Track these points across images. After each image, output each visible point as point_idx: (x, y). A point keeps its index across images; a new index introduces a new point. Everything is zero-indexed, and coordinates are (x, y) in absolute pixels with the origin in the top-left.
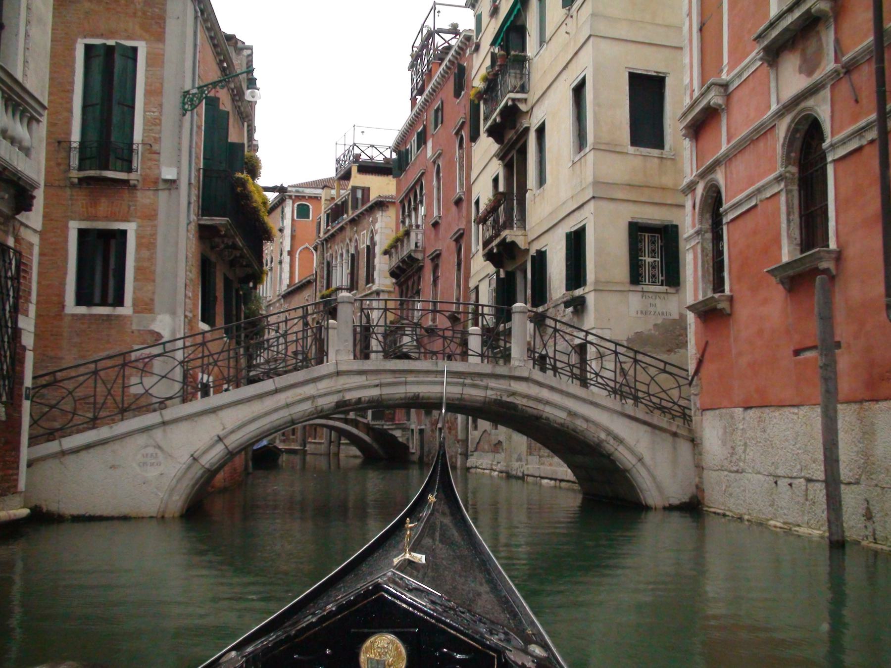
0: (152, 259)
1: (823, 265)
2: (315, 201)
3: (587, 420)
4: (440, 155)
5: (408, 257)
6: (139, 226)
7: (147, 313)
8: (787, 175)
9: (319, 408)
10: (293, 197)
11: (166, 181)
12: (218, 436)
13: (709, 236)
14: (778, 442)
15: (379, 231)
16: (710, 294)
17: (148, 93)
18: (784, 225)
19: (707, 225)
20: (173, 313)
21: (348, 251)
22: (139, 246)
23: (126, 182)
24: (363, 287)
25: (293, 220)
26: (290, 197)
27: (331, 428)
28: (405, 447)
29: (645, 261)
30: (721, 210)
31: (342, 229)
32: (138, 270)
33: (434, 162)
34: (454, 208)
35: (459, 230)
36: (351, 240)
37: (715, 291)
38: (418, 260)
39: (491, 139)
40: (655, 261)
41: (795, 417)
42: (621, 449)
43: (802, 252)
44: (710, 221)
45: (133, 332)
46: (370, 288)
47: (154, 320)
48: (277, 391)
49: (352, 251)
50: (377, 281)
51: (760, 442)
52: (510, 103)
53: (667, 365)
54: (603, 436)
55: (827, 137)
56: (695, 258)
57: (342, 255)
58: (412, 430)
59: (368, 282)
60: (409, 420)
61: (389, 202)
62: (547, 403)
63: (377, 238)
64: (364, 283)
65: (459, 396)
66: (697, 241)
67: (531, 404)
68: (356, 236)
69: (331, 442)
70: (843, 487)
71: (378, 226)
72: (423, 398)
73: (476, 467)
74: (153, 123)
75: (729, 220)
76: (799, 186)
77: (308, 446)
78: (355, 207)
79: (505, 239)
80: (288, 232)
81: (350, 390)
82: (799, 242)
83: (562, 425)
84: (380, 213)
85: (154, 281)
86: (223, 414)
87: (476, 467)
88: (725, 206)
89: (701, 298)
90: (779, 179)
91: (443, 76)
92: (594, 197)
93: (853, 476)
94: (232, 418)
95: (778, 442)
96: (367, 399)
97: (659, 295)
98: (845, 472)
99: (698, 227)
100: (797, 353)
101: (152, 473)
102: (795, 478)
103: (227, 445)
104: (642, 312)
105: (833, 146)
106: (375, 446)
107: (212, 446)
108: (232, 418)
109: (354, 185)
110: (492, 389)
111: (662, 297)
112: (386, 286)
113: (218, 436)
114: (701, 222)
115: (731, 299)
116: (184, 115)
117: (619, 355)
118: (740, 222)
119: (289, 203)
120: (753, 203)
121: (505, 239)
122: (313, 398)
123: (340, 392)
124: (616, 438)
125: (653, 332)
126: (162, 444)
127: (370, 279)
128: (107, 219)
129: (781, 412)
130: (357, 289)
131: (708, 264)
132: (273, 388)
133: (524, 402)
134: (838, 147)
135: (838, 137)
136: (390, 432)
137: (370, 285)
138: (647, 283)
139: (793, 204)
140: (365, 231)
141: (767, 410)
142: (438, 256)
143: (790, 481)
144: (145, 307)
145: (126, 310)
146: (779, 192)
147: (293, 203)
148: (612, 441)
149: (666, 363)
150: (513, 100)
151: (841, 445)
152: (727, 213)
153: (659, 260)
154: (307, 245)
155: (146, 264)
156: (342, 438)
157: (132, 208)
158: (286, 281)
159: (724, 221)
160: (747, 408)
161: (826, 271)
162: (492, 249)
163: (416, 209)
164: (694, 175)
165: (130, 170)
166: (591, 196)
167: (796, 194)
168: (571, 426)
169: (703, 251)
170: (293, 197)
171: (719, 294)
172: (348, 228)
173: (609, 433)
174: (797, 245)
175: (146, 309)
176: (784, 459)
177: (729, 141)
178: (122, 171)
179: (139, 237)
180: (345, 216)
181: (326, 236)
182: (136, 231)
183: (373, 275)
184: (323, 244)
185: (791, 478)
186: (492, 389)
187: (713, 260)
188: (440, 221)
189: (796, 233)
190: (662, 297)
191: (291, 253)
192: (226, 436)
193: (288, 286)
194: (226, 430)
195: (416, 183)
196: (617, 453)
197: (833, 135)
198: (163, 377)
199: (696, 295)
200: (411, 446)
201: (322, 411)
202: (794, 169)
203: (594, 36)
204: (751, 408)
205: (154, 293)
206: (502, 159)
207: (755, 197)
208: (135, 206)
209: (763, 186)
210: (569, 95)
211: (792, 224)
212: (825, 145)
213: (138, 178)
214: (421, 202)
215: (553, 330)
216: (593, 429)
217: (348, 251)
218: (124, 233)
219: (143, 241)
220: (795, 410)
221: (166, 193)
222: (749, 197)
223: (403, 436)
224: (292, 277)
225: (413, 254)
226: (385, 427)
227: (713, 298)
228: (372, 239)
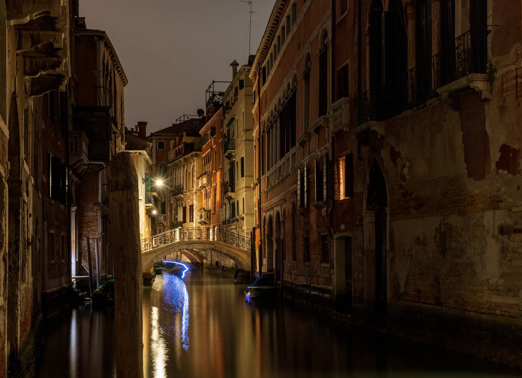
10: (156, 139)
25: (156, 149)
140: (190, 164)
150: (230, 152)
170: (156, 139)
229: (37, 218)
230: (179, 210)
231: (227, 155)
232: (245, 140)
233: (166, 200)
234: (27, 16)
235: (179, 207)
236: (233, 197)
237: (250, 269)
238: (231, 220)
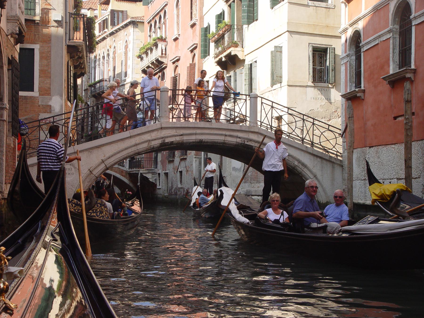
0: (49, 65)
1: (408, 75)
5: (156, 61)
6: (41, 47)
7: (47, 95)
8: (394, 29)
9: (152, 147)
12: (102, 160)
13: (354, 58)
14: (385, 163)
16: (353, 89)
18: (391, 55)
19: (353, 52)
22: (41, 58)
29: (316, 68)
30: (361, 45)
32: (41, 71)
34: (190, 30)
35: (194, 44)
37: (356, 87)
40: (321, 68)
41: (393, 149)
42: (305, 170)
43: (399, 69)
44: (354, 50)
45: (39, 106)
47: (51, 99)
48: (131, 137)
51: (377, 163)
53: (330, 127)
54: (296, 163)
55: (413, 13)
56: (346, 69)
58: (159, 174)
60: (156, 168)
61: (138, 22)
65: (223, 141)
66: (347, 60)
70: (413, 180)
72: (204, 142)
75: (364, 51)
76: (400, 35)
78: (113, 24)
82: (398, 64)
85: (50, 77)
86: (104, 148)
88: (363, 43)
89: (348, 91)
90: (390, 31)
93: (418, 174)
94: (109, 151)
95: (385, 163)
96: (176, 142)
97: (324, 88)
98: (414, 173)
99: (348, 52)
100: (395, 118)
102: (392, 179)
103: (106, 164)
104: (314, 98)
105: (415, 18)
107: (99, 165)
108: (109, 151)
110: (240, 138)
111: (325, 90)
113: (102, 160)
114: (350, 51)
115: (364, 91)
117: (305, 121)
118: (370, 51)
120: (377, 43)
121: (230, 53)
122: (149, 141)
123: (162, 138)
124: (303, 164)
125: (319, 109)
129: (386, 148)
131: (353, 73)
132: (129, 135)
134: (417, 18)
135: (417, 14)
138: (317, 81)
139: (396, 45)
140: (121, 41)
141: (380, 147)
142: (178, 60)
143: (390, 181)
145: (35, 93)
146: (389, 38)
148: (301, 166)
149: (329, 125)
151: (413, 160)
152: (363, 47)
153: (324, 68)
155: (46, 68)
157: (37, 36)
159: (362, 50)
160: (370, 147)
161: (409, 79)
162: (222, 58)
164: (346, 24)
166: (287, 30)
167: (398, 40)
169: (350, 66)
171: (359, 89)
173: (299, 161)
174: (397, 65)
175: (46, 93)
176: (387, 171)
177: (365, 10)
179: (41, 53)
182: (39, 49)
185: (391, 179)
186: (240, 138)
187: (356, 71)
188: (179, 37)
189: (397, 58)
190: (325, 90)
192: (106, 160)
194: (106, 157)
196: (303, 172)
197: (415, 13)
198: (240, 110)
199: (346, 90)
200: (158, 184)
201: (153, 148)
202: (397, 27)
204: (373, 147)
205: (50, 84)
207: (378, 39)
208: (38, 35)
209: (382, 34)
211: (395, 54)
212: (411, 17)
215: (271, 107)
218: (33, 49)
219: (44, 55)
220: (393, 146)
222: (375, 39)
225: (160, 59)
227: (355, 90)
236: (241, 57)
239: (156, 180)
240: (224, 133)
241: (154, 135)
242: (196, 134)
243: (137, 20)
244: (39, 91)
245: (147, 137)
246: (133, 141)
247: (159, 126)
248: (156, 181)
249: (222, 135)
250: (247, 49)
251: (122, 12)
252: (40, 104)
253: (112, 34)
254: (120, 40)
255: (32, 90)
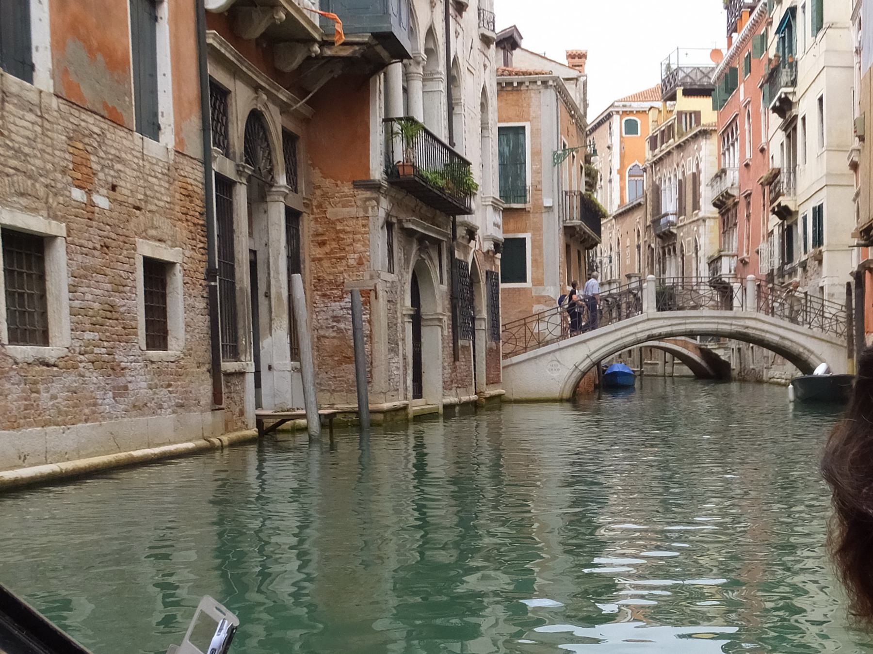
0: (541, 254)
2: (641, 115)
3: (791, 341)
4: (749, 102)
6: (532, 235)
10: (621, 113)
11: (546, 207)
15: (703, 159)
17: (533, 154)
20: (555, 285)
21: (675, 175)
23: (524, 209)
24: (690, 213)
25: (621, 136)
26: (618, 112)
27: (666, 350)
28: (727, 365)
31: (669, 153)
33: (745, 106)
34: (760, 154)
36: (678, 166)
38: (733, 196)
39: (776, 115)
42: (812, 357)
46: (697, 214)
47: (544, 290)
48: (616, 330)
49: (680, 177)
50: (703, 208)
52: (783, 96)
54: (801, 350)
57: (670, 179)
59: (694, 209)
61: (712, 130)
62: (767, 332)
63: (701, 166)
64: (691, 209)
67: (758, 333)
68: (683, 161)
69: (666, 362)
71: (702, 153)
73: (773, 378)
74: (537, 172)
77: (644, 366)
79: (780, 204)
80: (616, 149)
81: (654, 328)
83: (777, 344)
84: (704, 140)
87: (773, 378)
91: (750, 30)
92: (826, 185)
94: (593, 345)
101: (555, 375)
106: (703, 364)
108: (593, 345)
109: (679, 109)
112: (712, 213)
116: (554, 166)
119: (616, 119)
122: (635, 333)
124: (809, 351)
126: (560, 360)
127: (696, 206)
128: (514, 231)
130: (685, 215)
133: (754, 331)
136: (714, 351)
137: (697, 211)
140: (691, 158)
142: (749, 195)
144: (538, 282)
145: (528, 284)
147: (621, 119)
148: (807, 353)
150: (786, 94)
154: (636, 162)
156: (675, 358)
158: (617, 202)
163: (733, 145)
165: (525, 202)
168: (782, 345)
170: (621, 113)
172: (675, 153)
173: (805, 348)
178: (521, 203)
179: (533, 242)
180: (672, 140)
181: (655, 159)
183: (699, 202)
184: (652, 167)
188: (751, 163)
191: (621, 172)
192: (591, 355)
193: (619, 206)
195: (728, 127)
203: (828, 67)
206: (785, 130)
210: (817, 102)
213: (531, 206)
214: (737, 139)
216: (795, 346)
217: (675, 175)
221: (547, 214)
223: (725, 354)
224: (622, 198)
225: (729, 191)
226: (709, 347)
228: (698, 165)
229: (376, 298)
230: (668, 263)
231: (778, 104)
232: (826, 51)
233: (641, 241)
234: (680, 359)
235: (667, 256)
236: (792, 208)
237: (334, 431)
238: (787, 267)
239: (729, 357)
240: (716, 321)
241: (640, 327)
242: (685, 324)
243: (711, 128)
244: (532, 282)
245: (633, 329)
246: (619, 334)
247: (646, 318)
248: (730, 359)
249: (714, 323)
250: (801, 197)
251: (695, 112)
252: (533, 294)
253: (679, 147)
254: (689, 157)
255: (525, 281)
